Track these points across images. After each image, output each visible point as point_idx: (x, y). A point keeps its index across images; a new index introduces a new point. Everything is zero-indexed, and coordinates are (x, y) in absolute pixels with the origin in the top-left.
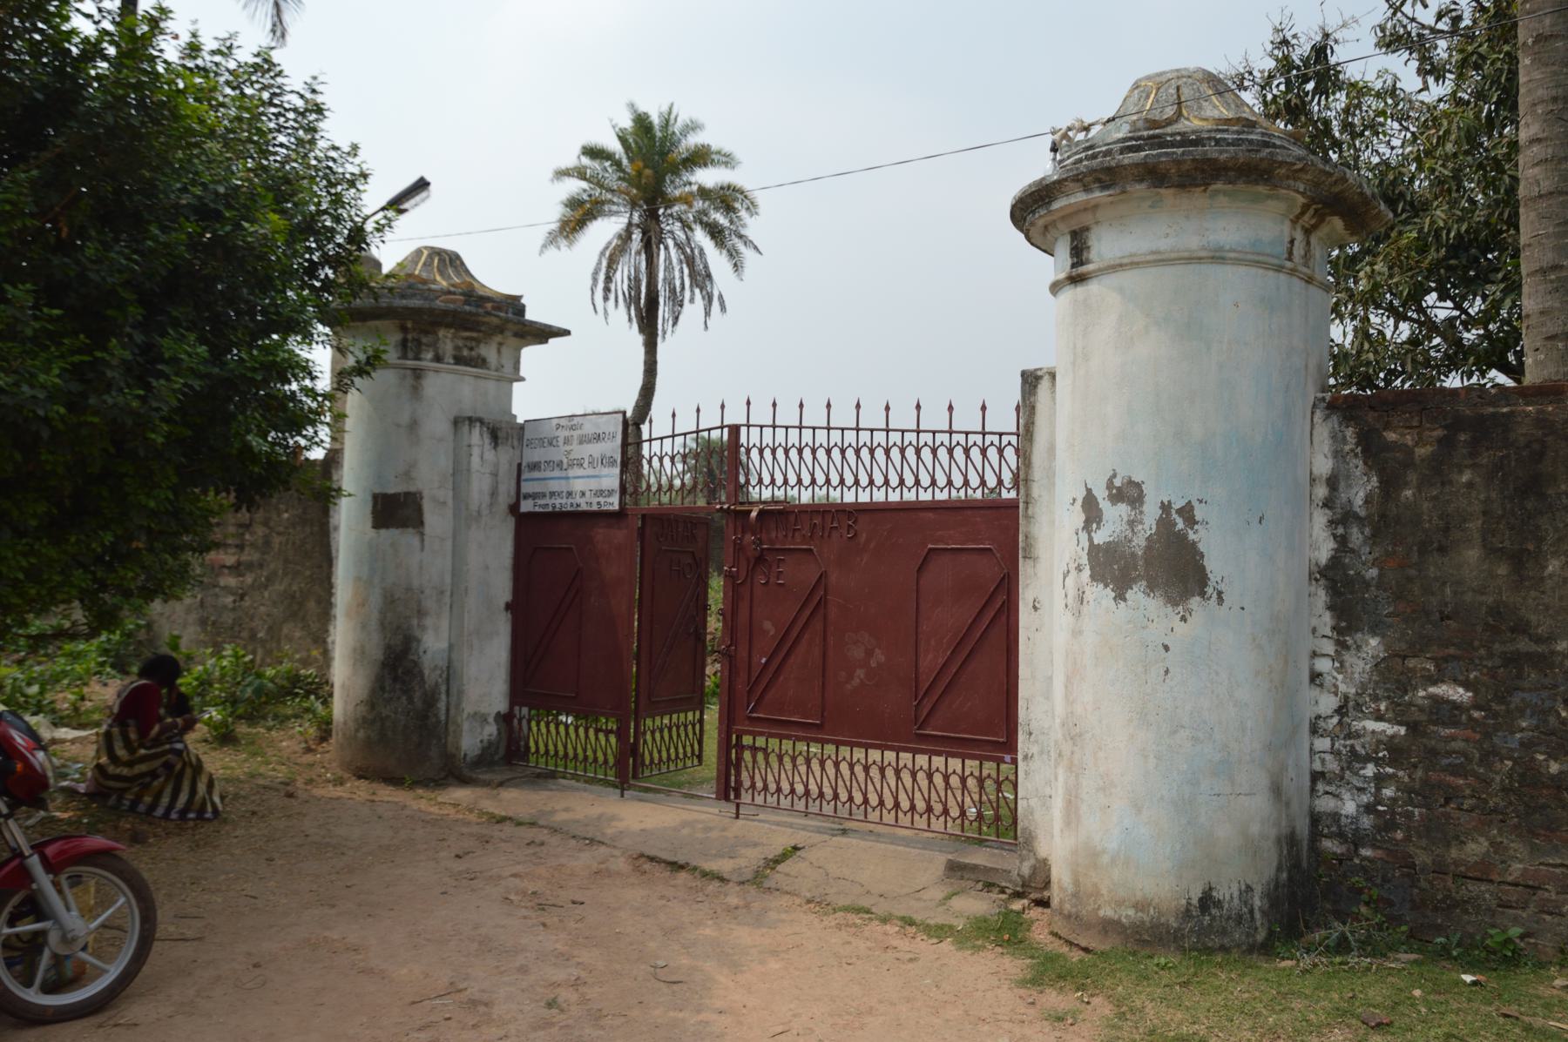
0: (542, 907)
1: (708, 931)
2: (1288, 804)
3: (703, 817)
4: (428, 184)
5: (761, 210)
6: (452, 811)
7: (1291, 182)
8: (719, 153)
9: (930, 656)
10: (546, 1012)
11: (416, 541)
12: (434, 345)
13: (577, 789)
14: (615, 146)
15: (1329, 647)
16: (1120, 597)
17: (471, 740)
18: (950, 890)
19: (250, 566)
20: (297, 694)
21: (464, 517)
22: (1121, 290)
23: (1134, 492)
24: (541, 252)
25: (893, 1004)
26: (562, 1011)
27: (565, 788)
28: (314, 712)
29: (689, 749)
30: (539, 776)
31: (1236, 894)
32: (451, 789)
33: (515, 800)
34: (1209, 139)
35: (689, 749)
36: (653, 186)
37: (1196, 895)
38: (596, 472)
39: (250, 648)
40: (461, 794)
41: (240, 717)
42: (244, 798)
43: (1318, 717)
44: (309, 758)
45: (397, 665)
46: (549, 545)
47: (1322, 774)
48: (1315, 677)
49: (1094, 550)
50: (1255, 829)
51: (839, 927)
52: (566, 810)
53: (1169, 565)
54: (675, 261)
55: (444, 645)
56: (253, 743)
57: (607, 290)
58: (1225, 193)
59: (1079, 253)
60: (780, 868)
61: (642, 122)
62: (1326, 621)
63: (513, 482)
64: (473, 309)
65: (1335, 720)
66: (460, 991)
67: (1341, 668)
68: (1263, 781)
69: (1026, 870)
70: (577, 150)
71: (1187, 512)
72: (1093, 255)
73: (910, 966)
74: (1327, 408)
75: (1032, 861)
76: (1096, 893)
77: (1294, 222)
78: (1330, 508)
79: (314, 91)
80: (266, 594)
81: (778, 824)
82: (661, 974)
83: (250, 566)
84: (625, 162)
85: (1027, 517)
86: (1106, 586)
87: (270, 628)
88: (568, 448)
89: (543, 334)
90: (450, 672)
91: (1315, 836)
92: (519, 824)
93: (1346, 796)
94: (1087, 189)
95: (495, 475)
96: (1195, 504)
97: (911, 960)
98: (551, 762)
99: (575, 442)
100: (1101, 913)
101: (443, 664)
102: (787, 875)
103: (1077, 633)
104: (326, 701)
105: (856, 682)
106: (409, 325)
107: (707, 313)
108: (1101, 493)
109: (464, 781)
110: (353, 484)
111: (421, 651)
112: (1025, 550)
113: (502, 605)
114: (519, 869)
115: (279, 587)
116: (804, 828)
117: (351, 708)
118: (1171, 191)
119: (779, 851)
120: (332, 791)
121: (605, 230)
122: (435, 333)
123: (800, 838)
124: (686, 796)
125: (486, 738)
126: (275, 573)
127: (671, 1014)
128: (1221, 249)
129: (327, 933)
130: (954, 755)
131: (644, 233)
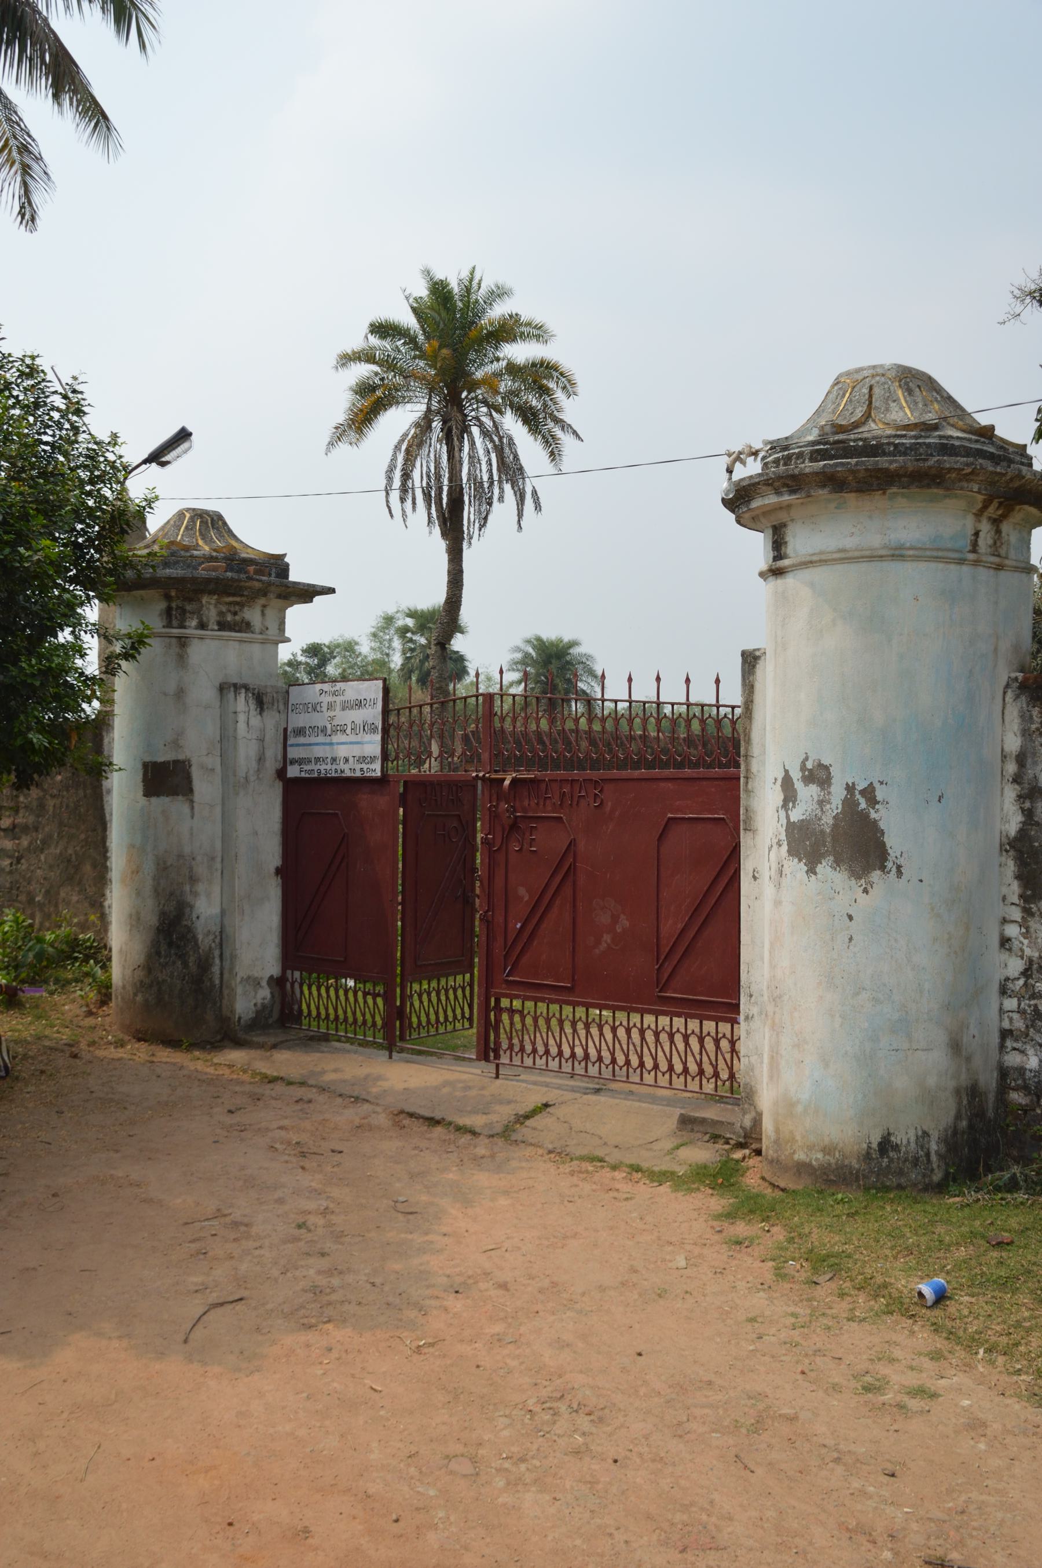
0: (303, 1155)
1: (451, 1176)
2: (968, 1059)
3: (465, 1077)
4: (190, 434)
5: (580, 388)
6: (227, 1071)
7: (965, 484)
8: (528, 324)
9: (670, 922)
10: (296, 1232)
11: (186, 809)
12: (198, 612)
13: (349, 1051)
14: (409, 320)
15: (1016, 914)
16: (811, 871)
17: (245, 1003)
18: (680, 1141)
19: (25, 829)
20: (76, 958)
21: (232, 783)
22: (812, 585)
23: (823, 775)
24: (328, 451)
25: (596, 1231)
26: (310, 1231)
27: (337, 1050)
28: (94, 976)
29: (458, 1011)
30: (311, 1038)
31: (913, 1139)
32: (226, 1051)
33: (288, 1062)
34: (889, 444)
35: (458, 1011)
36: (455, 373)
37: (876, 1139)
38: (358, 738)
39: (29, 912)
40: (236, 1056)
41: (23, 982)
42: (33, 1058)
43: (1007, 979)
44: (90, 1021)
45: (171, 932)
46: (315, 807)
47: (1010, 1032)
48: (1005, 942)
49: (790, 827)
50: (932, 1081)
51: (572, 1173)
52: (335, 1071)
53: (854, 842)
54: (481, 452)
55: (216, 910)
56: (37, 1007)
57: (404, 490)
58: (903, 495)
59: (778, 546)
60: (528, 1123)
61: (440, 290)
62: (1014, 889)
63: (280, 747)
64: (235, 576)
65: (1021, 982)
66: (225, 1216)
67: (1027, 935)
68: (941, 1037)
69: (747, 1122)
70: (365, 328)
71: (869, 793)
72: (790, 550)
73: (625, 1203)
74: (1019, 688)
75: (753, 1114)
76: (793, 1140)
77: (979, 515)
78: (1019, 783)
79: (74, 391)
80: (42, 857)
81: (535, 1083)
82: (400, 1206)
83: (25, 829)
84: (421, 338)
85: (747, 791)
86: (800, 860)
87: (47, 892)
88: (332, 714)
89: (307, 593)
90: (223, 938)
91: (1003, 1088)
92: (290, 1083)
93: (1031, 1052)
94: (778, 493)
95: (261, 740)
96: (877, 785)
97: (627, 1199)
98: (314, 1024)
99: (338, 708)
100: (796, 1157)
101: (216, 929)
102: (535, 1129)
103: (778, 903)
104: (105, 966)
105: (603, 946)
106: (173, 594)
107: (520, 515)
108: (796, 775)
109: (239, 1043)
110: (122, 748)
111: (194, 916)
112: (745, 822)
113: (272, 870)
114: (286, 1122)
115: (55, 850)
116: (559, 1087)
117: (128, 972)
118: (853, 494)
119: (531, 1107)
120: (113, 1053)
121: (398, 421)
122: (199, 601)
123: (551, 1096)
124: (458, 1058)
125: (259, 1001)
126: (50, 836)
127: (403, 1235)
128: (901, 547)
129: (112, 1172)
130: (693, 1016)
131: (445, 422)
